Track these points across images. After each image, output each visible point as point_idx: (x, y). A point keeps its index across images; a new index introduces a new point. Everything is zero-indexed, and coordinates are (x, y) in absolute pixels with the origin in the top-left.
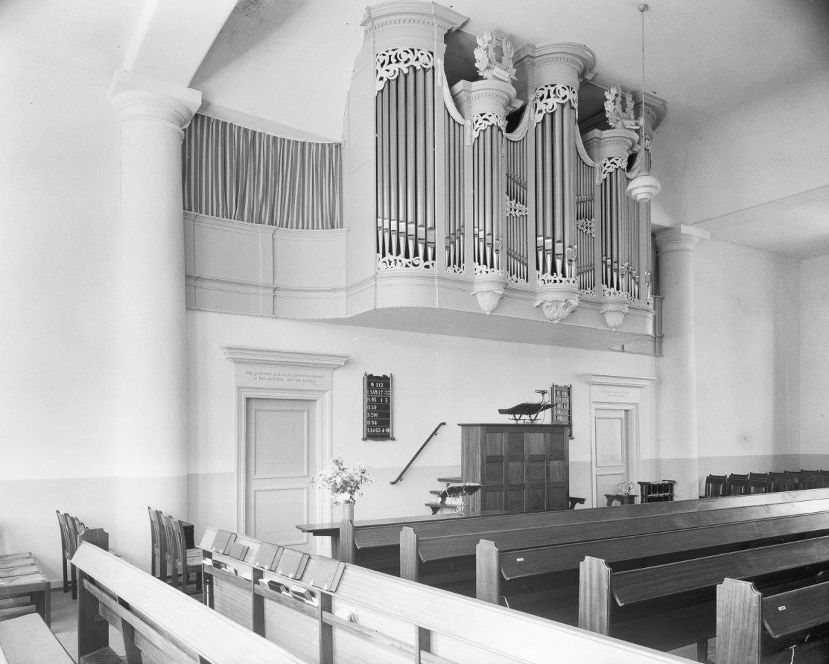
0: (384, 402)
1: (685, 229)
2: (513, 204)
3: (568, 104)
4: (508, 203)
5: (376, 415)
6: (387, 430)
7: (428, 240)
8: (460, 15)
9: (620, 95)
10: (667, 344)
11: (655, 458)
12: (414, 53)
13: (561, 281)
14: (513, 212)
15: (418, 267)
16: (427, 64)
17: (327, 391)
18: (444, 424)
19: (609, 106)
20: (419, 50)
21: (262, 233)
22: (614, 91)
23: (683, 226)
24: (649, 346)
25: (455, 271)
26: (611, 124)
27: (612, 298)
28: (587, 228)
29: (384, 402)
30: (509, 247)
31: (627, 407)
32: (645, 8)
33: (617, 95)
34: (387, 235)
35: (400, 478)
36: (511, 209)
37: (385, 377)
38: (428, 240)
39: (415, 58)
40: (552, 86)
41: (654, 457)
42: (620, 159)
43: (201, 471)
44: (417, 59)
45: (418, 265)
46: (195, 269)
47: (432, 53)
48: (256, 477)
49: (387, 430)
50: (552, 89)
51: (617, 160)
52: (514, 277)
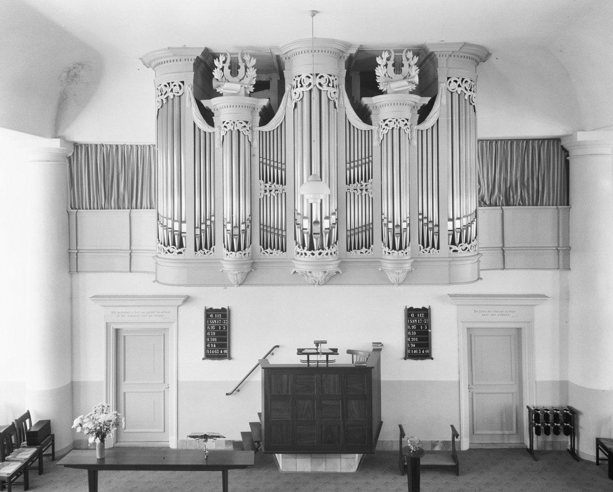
0: (222, 329)
1: (581, 136)
2: (268, 187)
3: (315, 88)
4: (263, 187)
5: (215, 340)
6: (225, 351)
7: (182, 231)
8: (196, 48)
9: (392, 58)
10: (574, 258)
11: (559, 380)
12: (169, 86)
13: (306, 254)
14: (268, 193)
15: (173, 253)
16: (178, 93)
17: (173, 322)
18: (278, 346)
19: (379, 71)
20: (172, 83)
21: (122, 215)
22: (385, 55)
23: (579, 133)
24: (550, 258)
25: (205, 254)
26: (381, 88)
27: (390, 257)
28: (362, 190)
29: (222, 329)
30: (262, 223)
31: (518, 326)
32: (314, 13)
33: (388, 59)
34: (279, 171)
35: (237, 390)
36: (266, 191)
37: (223, 309)
38: (182, 231)
39: (170, 89)
40: (299, 76)
41: (557, 378)
42: (395, 120)
43: (82, 380)
44: (172, 90)
45: (172, 252)
46: (77, 246)
47: (183, 82)
48: (126, 382)
49: (225, 351)
50: (298, 79)
51: (390, 121)
52: (269, 250)
